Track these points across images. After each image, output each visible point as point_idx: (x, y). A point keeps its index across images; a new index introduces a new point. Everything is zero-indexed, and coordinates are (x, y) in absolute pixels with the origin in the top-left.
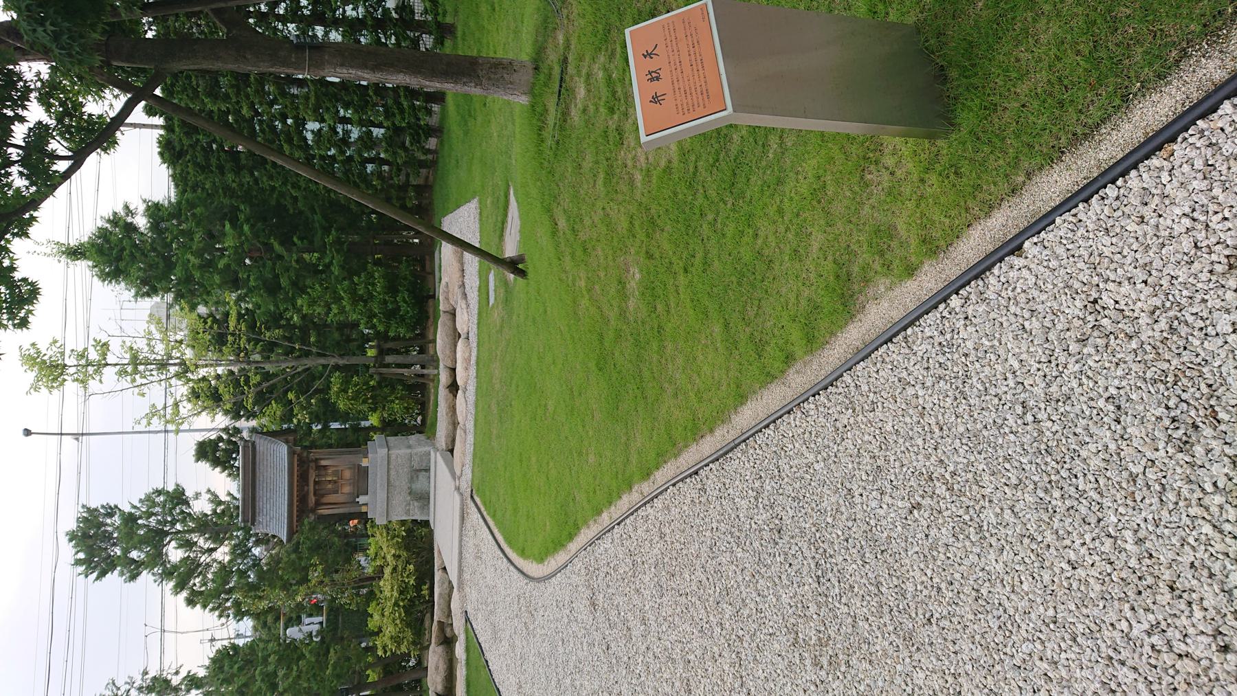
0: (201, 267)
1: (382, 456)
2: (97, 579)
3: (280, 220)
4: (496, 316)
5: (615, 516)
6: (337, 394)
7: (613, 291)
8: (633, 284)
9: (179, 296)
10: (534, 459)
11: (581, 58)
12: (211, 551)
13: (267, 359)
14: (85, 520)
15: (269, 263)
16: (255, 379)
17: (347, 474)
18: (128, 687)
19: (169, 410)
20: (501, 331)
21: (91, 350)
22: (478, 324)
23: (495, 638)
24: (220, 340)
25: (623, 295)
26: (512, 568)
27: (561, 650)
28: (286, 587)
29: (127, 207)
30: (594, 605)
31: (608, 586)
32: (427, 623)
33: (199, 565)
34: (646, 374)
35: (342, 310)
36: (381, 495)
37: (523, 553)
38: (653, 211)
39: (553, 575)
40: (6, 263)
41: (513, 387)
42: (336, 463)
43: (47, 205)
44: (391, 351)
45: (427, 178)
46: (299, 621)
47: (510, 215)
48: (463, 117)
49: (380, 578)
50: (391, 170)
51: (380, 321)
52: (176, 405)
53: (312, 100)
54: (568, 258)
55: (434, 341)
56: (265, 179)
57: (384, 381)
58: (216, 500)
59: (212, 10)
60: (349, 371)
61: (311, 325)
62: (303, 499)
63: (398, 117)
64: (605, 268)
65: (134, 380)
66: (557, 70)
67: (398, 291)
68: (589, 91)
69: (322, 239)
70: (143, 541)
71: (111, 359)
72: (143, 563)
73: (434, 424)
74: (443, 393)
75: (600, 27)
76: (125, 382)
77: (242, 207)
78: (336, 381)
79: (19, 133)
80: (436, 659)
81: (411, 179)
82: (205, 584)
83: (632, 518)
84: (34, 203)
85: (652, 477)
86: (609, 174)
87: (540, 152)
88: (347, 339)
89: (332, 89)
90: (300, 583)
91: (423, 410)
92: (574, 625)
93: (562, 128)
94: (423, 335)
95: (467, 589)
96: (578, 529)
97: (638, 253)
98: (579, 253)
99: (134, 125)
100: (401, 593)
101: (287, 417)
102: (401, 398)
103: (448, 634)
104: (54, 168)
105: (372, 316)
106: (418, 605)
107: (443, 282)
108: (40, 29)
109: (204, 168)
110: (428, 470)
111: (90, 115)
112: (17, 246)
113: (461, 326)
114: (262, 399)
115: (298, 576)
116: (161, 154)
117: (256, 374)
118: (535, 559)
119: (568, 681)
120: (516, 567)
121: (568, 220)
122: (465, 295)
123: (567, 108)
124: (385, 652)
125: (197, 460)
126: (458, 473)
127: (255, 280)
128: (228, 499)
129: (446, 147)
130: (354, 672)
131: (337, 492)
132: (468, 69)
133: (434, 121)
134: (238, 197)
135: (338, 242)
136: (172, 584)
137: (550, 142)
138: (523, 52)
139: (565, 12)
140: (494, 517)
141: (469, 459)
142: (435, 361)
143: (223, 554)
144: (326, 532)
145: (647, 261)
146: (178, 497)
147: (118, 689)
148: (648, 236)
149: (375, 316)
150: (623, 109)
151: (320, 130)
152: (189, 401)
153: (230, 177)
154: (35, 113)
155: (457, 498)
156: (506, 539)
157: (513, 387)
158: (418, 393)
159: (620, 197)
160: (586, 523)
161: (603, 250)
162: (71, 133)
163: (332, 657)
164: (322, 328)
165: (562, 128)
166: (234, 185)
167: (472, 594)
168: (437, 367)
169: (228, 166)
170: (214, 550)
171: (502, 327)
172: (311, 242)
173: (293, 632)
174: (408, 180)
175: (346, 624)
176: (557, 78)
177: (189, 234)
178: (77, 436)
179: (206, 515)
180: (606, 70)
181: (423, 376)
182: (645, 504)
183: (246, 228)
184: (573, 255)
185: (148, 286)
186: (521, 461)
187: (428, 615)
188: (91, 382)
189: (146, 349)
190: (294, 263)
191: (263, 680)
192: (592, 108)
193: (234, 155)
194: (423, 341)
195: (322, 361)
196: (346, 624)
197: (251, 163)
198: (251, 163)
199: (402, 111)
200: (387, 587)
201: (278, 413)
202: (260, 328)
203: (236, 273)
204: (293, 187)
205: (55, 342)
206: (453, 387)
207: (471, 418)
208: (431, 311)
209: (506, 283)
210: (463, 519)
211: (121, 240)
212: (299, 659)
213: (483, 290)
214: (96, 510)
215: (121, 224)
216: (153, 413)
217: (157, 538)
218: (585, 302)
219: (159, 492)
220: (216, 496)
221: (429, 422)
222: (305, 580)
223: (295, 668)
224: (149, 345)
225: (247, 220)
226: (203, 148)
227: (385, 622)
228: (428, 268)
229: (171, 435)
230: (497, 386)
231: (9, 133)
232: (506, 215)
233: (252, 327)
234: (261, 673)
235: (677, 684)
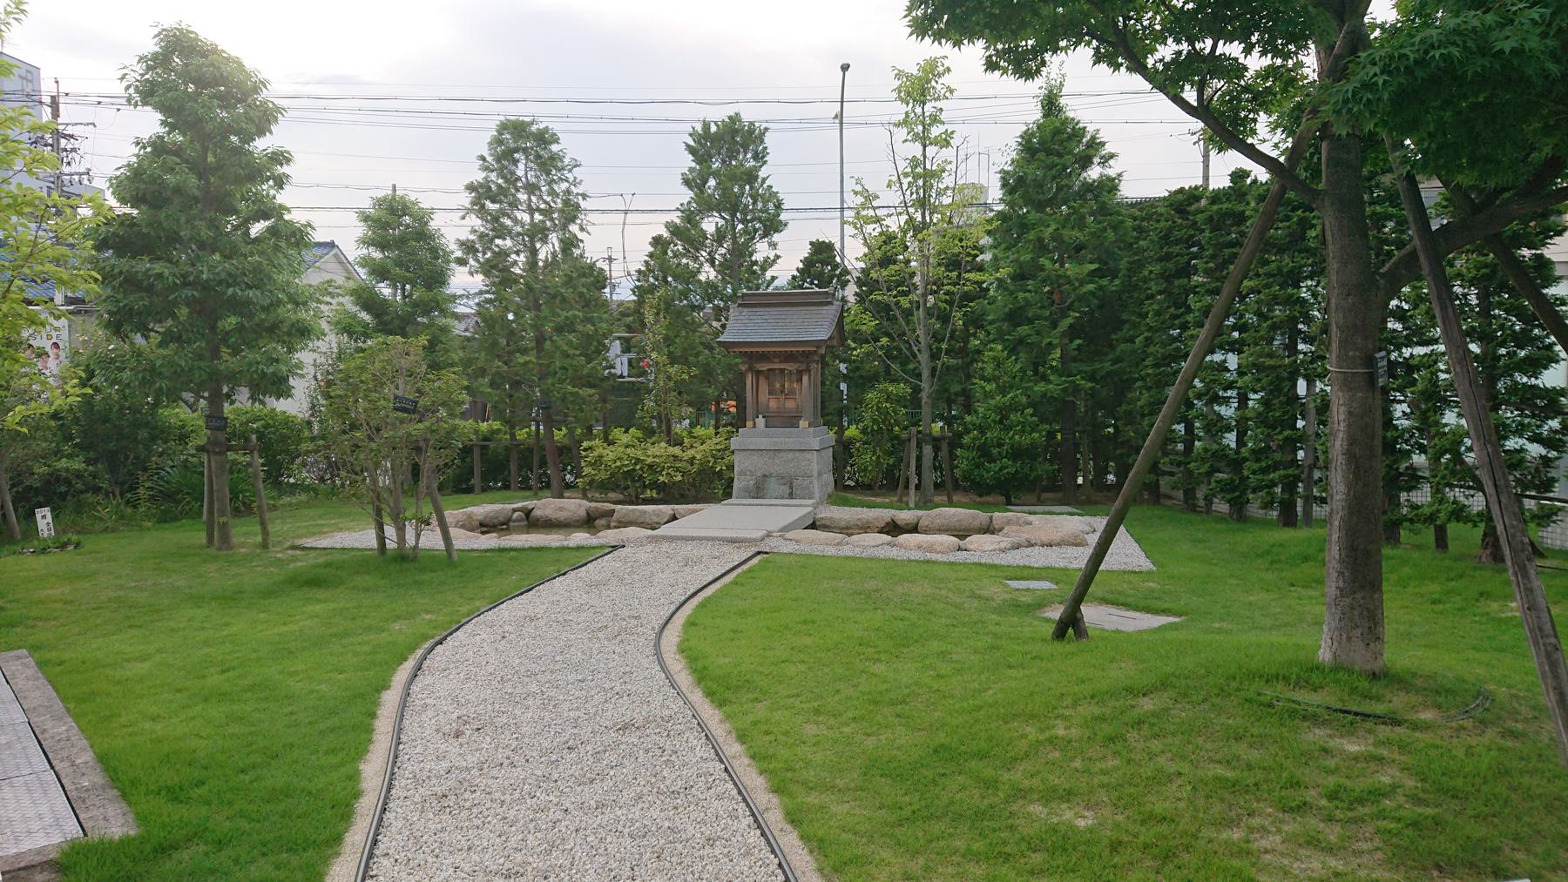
0: (1040, 240)
2: (688, 146)
3: (1100, 326)
4: (994, 590)
5: (736, 764)
6: (885, 391)
7: (1054, 780)
8: (1069, 815)
10: (808, 641)
11: (1403, 747)
12: (712, 261)
13: (929, 313)
14: (751, 132)
17: (790, 404)
19: (871, 212)
20: (974, 596)
21: (942, 129)
22: (981, 564)
23: (593, 585)
24: (953, 263)
25: (1051, 796)
26: (673, 607)
27: (572, 678)
28: (668, 340)
29: (1112, 156)
30: (624, 728)
31: (647, 751)
32: (612, 495)
33: (697, 250)
34: (937, 827)
36: (764, 443)
37: (691, 623)
38: (1186, 856)
39: (664, 668)
40: (1063, 44)
42: (805, 391)
43: (1138, 82)
44: (936, 449)
47: (1137, 614)
48: (1268, 552)
49: (668, 442)
50: (1177, 453)
51: (974, 439)
52: (878, 220)
54: (1097, 711)
55: (951, 504)
56: (1156, 307)
57: (898, 445)
58: (768, 263)
59: (1414, 251)
60: (915, 400)
62: (764, 357)
63: (1256, 466)
64: (1086, 771)
65: (906, 175)
66: (1380, 708)
67: (1015, 461)
68: (1356, 759)
69: (1080, 372)
71: (931, 150)
74: (885, 514)
75: (1460, 782)
76: (903, 166)
77: (1117, 282)
78: (901, 389)
79: (1234, 49)
80: (572, 507)
81: (1168, 478)
82: (675, 256)
83: (735, 792)
84: (1138, 66)
85: (789, 828)
86: (1233, 786)
87: (1252, 676)
88: (956, 398)
89: (1286, 385)
90: (670, 355)
91: (865, 487)
93: (1293, 714)
94: (957, 486)
95: (649, 548)
96: (721, 703)
97: (1117, 826)
98: (1107, 729)
99: (1206, 156)
100: (650, 466)
102: (878, 462)
104: (1187, 87)
105: (982, 430)
107: (1032, 518)
108: (1377, 69)
109: (1166, 238)
110: (791, 496)
111: (1255, 120)
112: (1085, 53)
113: (975, 540)
114: (883, 310)
116: (1182, 190)
118: (682, 642)
119: (534, 688)
121: (1154, 714)
123: (1325, 723)
125: (811, 243)
126: (788, 535)
127: (1025, 299)
130: (566, 415)
131: (771, 393)
132: (1363, 578)
133: (1254, 509)
135: (1077, 390)
136: (678, 221)
137: (1269, 693)
138: (1397, 655)
139: (1468, 723)
140: (735, 583)
141: (807, 549)
142: (925, 504)
143: (708, 274)
145: (1106, 842)
146: (773, 226)
148: (1146, 847)
149: (983, 433)
150: (1339, 814)
152: (881, 234)
153: (1157, 268)
154: (1256, 62)
155: (758, 534)
156: (708, 600)
157: (902, 613)
158: (888, 483)
159: (1201, 803)
160: (728, 717)
161: (1116, 769)
162: (1230, 101)
163: (585, 392)
165: (1293, 714)
166: (1146, 273)
167: (644, 554)
168: (917, 507)
169: (1170, 265)
170: (713, 264)
171: (979, 597)
172: (1075, 360)
173: (616, 347)
174: (1165, 473)
175: (622, 404)
176: (1367, 707)
177: (1081, 224)
178: (840, 116)
179: (751, 255)
180: (1394, 787)
181: (907, 487)
182: (753, 814)
183: (1091, 287)
184: (1101, 719)
185: (1014, 185)
186: (805, 622)
187: (621, 497)
188: (905, 130)
189: (942, 186)
190: (1047, 340)
192: (1331, 763)
193: (1187, 271)
194: (952, 486)
195: (926, 374)
196: (622, 404)
197: (1176, 291)
198: (1176, 291)
199: (1264, 471)
203: (1033, 277)
204: (1147, 339)
205: (952, 91)
208: (988, 499)
209: (1041, 604)
210: (732, 541)
211: (1070, 152)
212: (586, 356)
214: (762, 142)
215: (1092, 150)
216: (869, 197)
217: (730, 205)
218: (1032, 732)
219: (778, 206)
221: (849, 495)
222: (673, 360)
226: (1192, 236)
227: (620, 448)
228: (1045, 495)
230: (899, 589)
231: (1230, 39)
232: (1137, 609)
233: (968, 297)
234: (575, 317)
235: (519, 857)
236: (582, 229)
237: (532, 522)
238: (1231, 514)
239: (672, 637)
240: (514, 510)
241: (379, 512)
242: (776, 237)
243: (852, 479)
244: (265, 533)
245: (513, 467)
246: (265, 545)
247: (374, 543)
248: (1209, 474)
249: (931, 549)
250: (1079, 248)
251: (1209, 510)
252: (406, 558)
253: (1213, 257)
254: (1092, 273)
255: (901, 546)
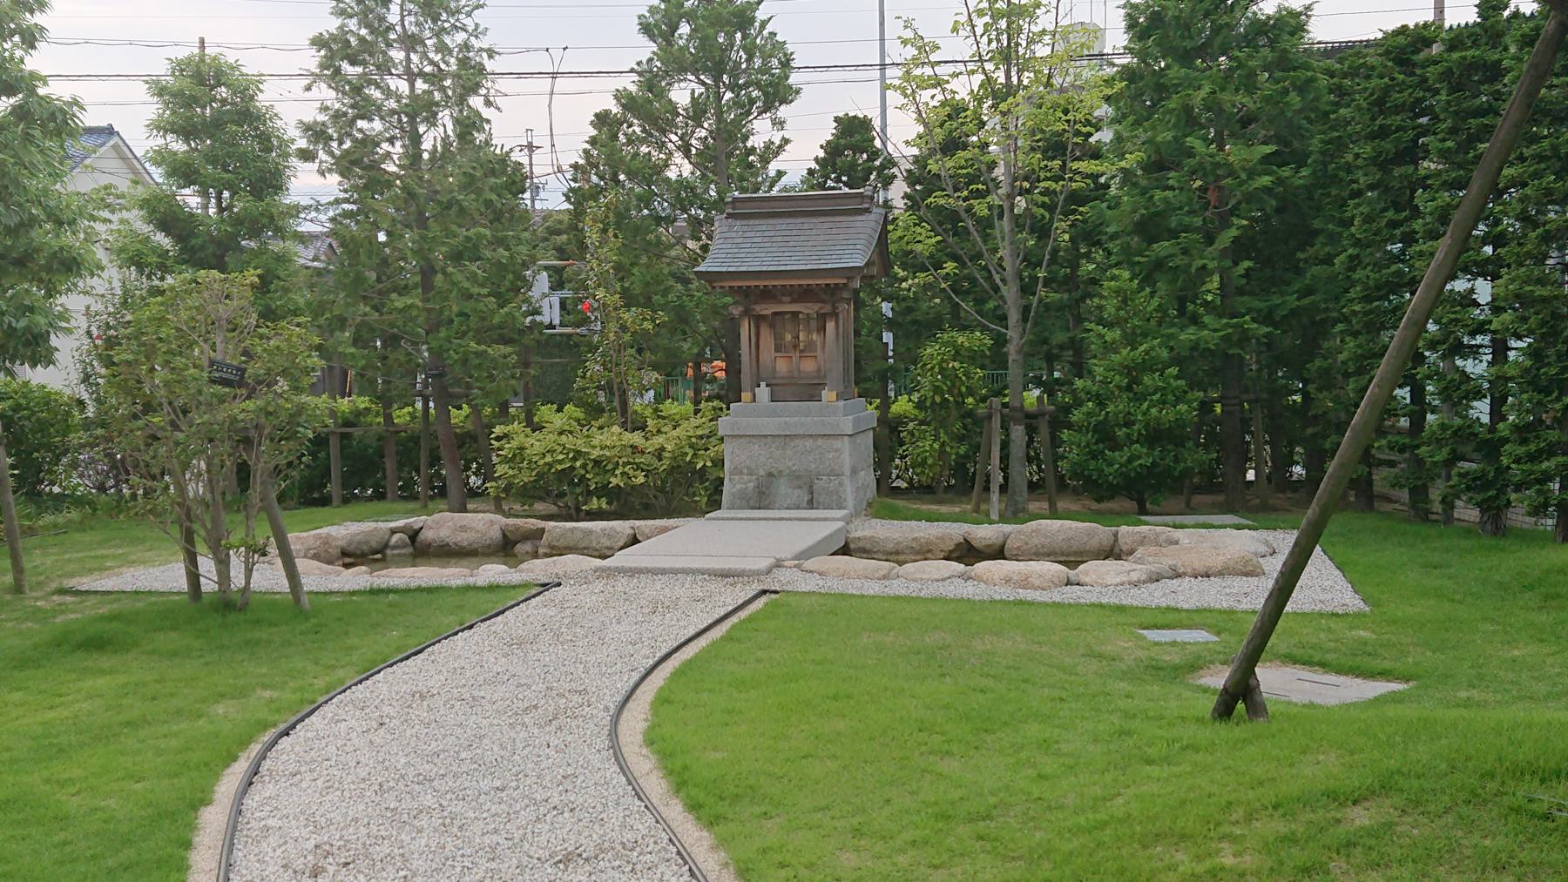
0: (1187, 109)
1: (843, 421)
3: (1280, 240)
6: (953, 344)
9: (1128, 74)
10: (841, 725)
12: (686, 149)
13: (1018, 223)
15: (1198, 221)
16: (980, 208)
17: (808, 366)
18: (470, 29)
19: (928, 71)
20: (1092, 655)
22: (1101, 606)
24: (1055, 147)
26: (636, 676)
27: (485, 784)
32: (540, 507)
33: (664, 132)
35: (1110, 348)
36: (770, 425)
37: (662, 700)
39: (624, 769)
41: (984, 682)
42: (829, 347)
44: (1031, 431)
45: (1389, 500)
46: (557, 285)
47: (1341, 679)
49: (624, 425)
50: (1400, 432)
52: (938, 83)
53: (1540, 291)
54: (1282, 827)
55: (1054, 514)
56: (1365, 209)
57: (973, 424)
58: (771, 151)
60: (997, 357)
61: (1079, 294)
62: (767, 295)
65: (981, 13)
67: (1151, 447)
70: (706, 43)
72: (669, 44)
73: (894, 514)
77: (1305, 172)
78: (976, 340)
80: (480, 526)
87: (1518, 773)
90: (625, 293)
92: (526, 815)
95: (599, 586)
96: (711, 822)
98: (1298, 856)
100: (597, 462)
101: (914, 265)
103: (519, 548)
106: (572, 491)
109: (1380, 104)
110: (811, 505)
114: (948, 220)
115: (637, 290)
117: (990, 208)
118: (651, 729)
119: (429, 800)
120: (637, 685)
121: (1370, 833)
122: (1156, 578)
124: (498, 439)
125: (837, 119)
126: (808, 564)
127: (1165, 199)
128: (772, 173)
129: (1467, 543)
133: (1518, 516)
134: (1325, 164)
135: (1244, 338)
136: (633, 88)
140: (728, 638)
141: (836, 586)
142: (1015, 514)
143: (681, 168)
144: (713, 333)
146: (778, 94)
147: (469, 15)
149: (1101, 404)
151: (1476, 304)
153: (1367, 150)
155: (763, 564)
156: (688, 664)
157: (984, 682)
158: (958, 482)
164: (1074, 312)
167: (590, 596)
168: (1003, 519)
169: (1388, 145)
170: (687, 155)
171: (1100, 656)
172: (1241, 292)
173: (542, 282)
174: (1381, 463)
175: (553, 366)
177: (1250, 85)
179: (746, 138)
181: (987, 489)
183: (1266, 180)
184: (1290, 839)
186: (835, 698)
190: (1200, 263)
191: (468, 239)
193: (1412, 154)
195: (1014, 316)
196: (553, 366)
197: (1396, 184)
198: (1396, 184)
199: (1533, 458)
200: (608, 438)
201: (919, 247)
202: (1074, 212)
203: (1176, 166)
206: (967, 553)
207: (912, 589)
209: (1195, 665)
210: (724, 574)
212: (498, 295)
213: (1172, 618)
216: (925, 48)
217: (712, 63)
219: (786, 64)
220: (777, 154)
222: (629, 300)
223: (484, 291)
224: (1044, 32)
225: (1280, 181)
226: (1419, 101)
227: (549, 436)
228: (1198, 499)
229: (877, 73)
232: (1340, 671)
233: (1076, 198)
234: (480, 236)
236: (488, 103)
237: (420, 549)
238: (1482, 523)
239: (635, 721)
240: (393, 531)
241: (189, 537)
242: (783, 111)
243: (903, 478)
244: (18, 570)
245: (390, 464)
246: (18, 588)
247: (183, 584)
248: (1450, 462)
249: (1025, 583)
250: (1247, 121)
251: (1448, 519)
252: (232, 606)
253: (1453, 131)
254: (1266, 159)
255: (979, 579)
